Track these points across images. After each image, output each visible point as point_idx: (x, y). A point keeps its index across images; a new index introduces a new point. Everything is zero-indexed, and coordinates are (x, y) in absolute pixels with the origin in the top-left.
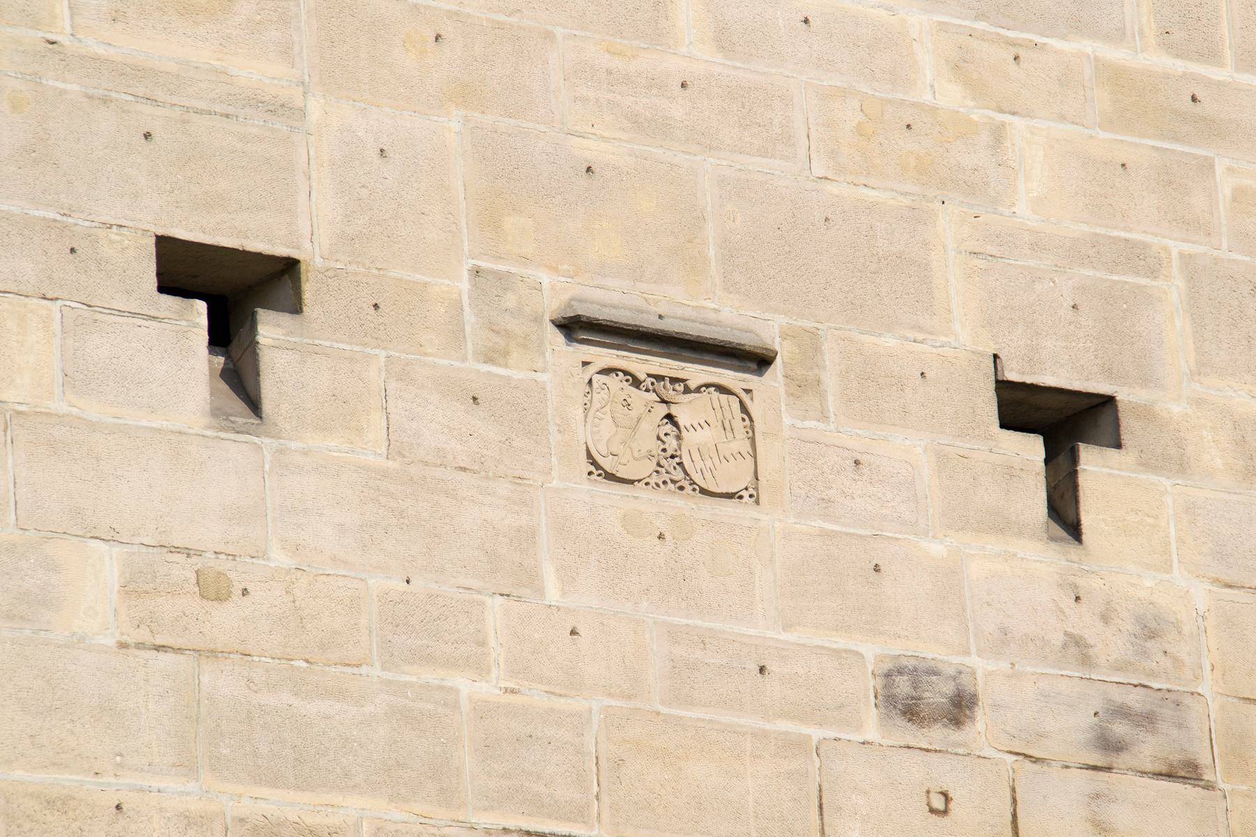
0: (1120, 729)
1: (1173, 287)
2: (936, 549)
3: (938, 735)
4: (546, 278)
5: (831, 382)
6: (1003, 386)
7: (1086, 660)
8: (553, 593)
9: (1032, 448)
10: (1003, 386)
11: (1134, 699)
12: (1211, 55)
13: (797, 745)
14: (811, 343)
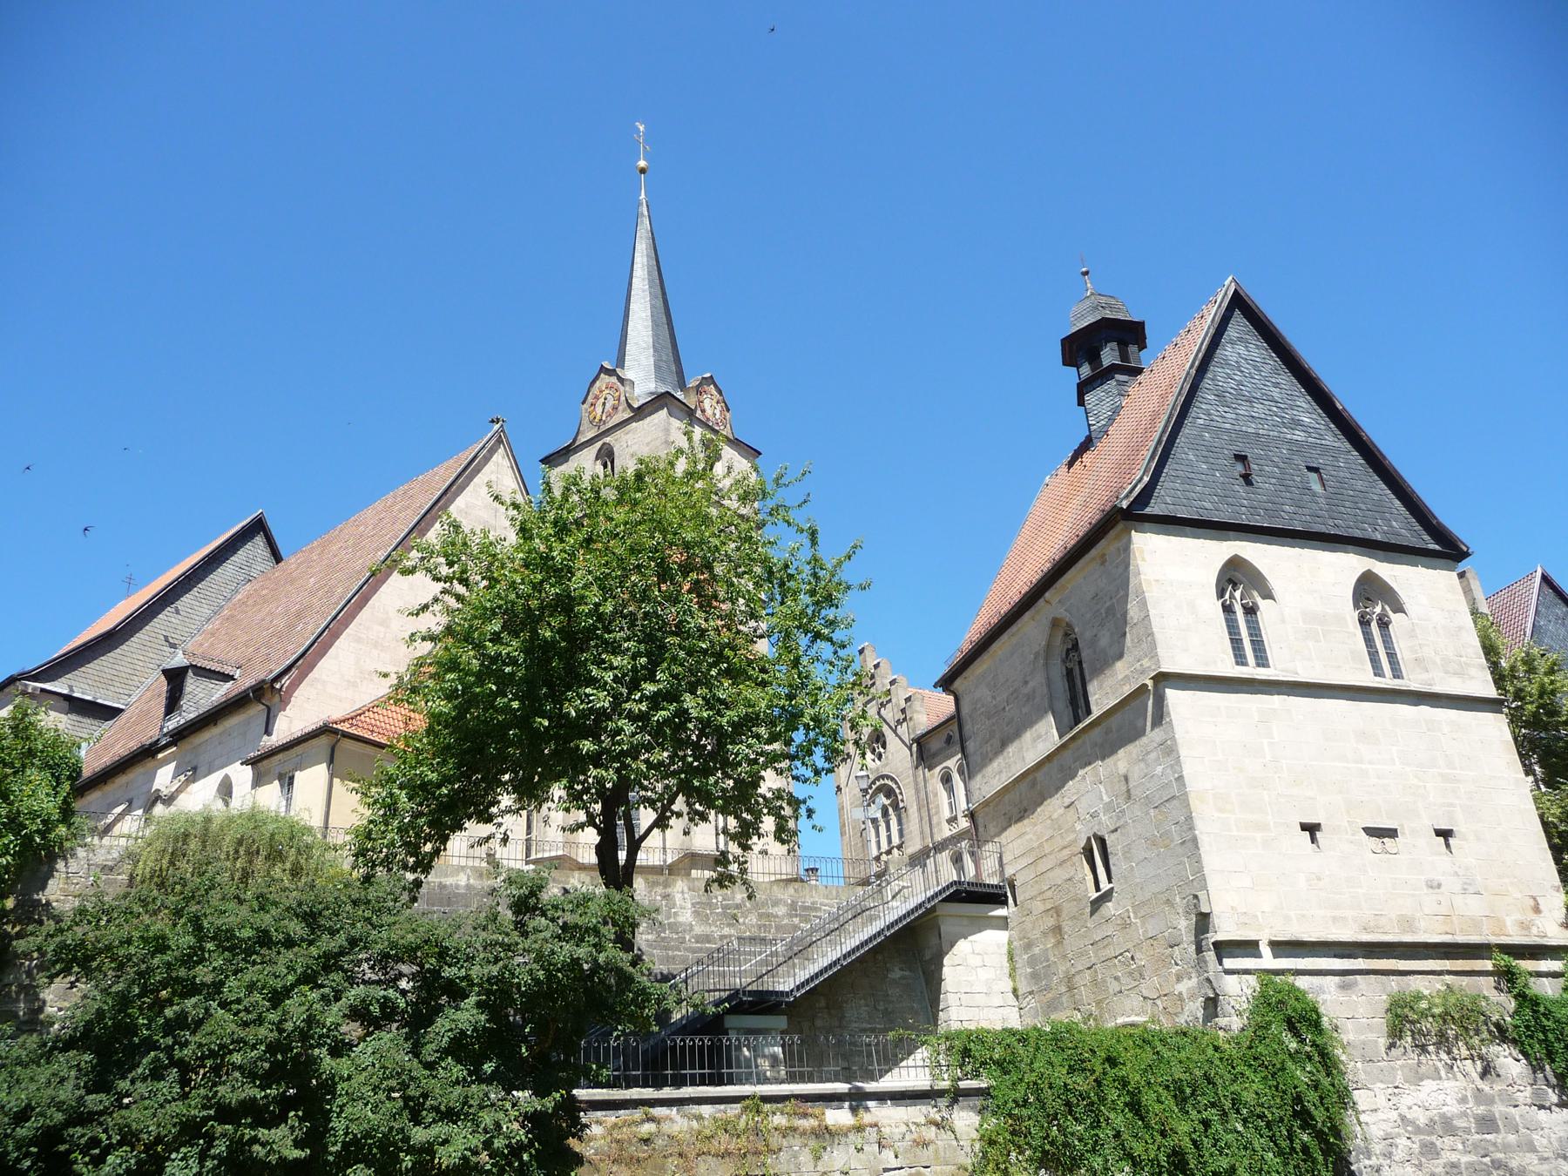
0: (1466, 886)
3: (1437, 890)
5: (1407, 832)
6: (1435, 830)
9: (1441, 839)
10: (1435, 830)
12: (1456, 769)
13: (1413, 895)
14: (1402, 826)
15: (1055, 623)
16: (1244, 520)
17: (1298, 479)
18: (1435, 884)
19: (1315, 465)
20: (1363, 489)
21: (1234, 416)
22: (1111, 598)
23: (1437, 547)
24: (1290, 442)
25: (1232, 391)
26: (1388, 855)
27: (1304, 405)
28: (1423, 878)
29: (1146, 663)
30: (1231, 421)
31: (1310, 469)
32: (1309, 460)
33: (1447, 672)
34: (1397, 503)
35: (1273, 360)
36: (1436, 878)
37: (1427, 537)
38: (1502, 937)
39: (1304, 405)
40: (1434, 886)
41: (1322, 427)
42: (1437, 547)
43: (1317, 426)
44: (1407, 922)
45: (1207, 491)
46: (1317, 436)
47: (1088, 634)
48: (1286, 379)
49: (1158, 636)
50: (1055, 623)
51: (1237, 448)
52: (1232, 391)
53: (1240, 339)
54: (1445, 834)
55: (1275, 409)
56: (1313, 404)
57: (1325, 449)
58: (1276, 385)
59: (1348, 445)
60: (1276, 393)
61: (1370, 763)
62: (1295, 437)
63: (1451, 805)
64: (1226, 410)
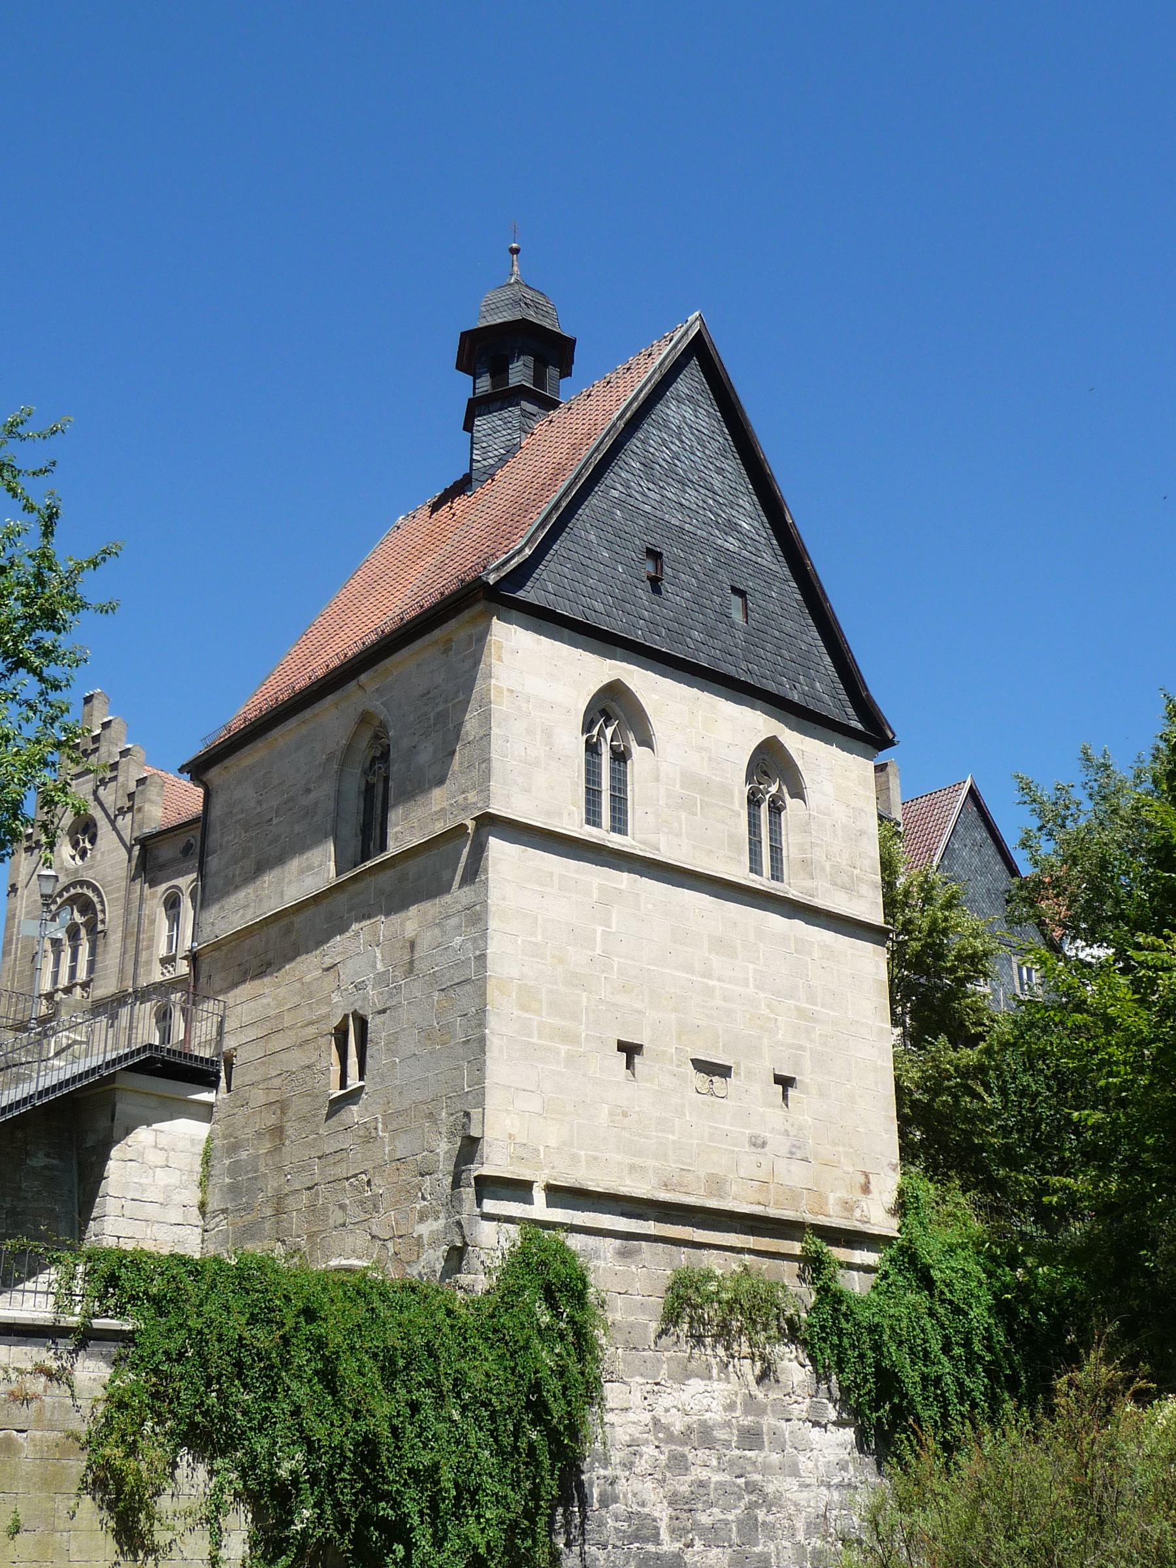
1: (807, 1054)
2: (761, 1110)
3: (759, 1150)
4: (689, 1049)
7: (788, 1135)
8: (688, 1118)
9: (780, 1088)
11: (796, 1143)
12: (816, 1005)
14: (738, 1064)
15: (365, 718)
16: (639, 636)
17: (718, 600)
18: (759, 1142)
19: (742, 587)
20: (792, 632)
21: (658, 497)
22: (446, 701)
23: (860, 726)
24: (720, 549)
25: (664, 464)
26: (713, 1099)
27: (747, 506)
28: (747, 1132)
29: (472, 797)
30: (653, 503)
31: (736, 591)
32: (737, 579)
33: (835, 884)
34: (827, 660)
35: (722, 438)
36: (763, 1134)
37: (851, 711)
38: (820, 1217)
39: (747, 506)
40: (758, 1143)
41: (763, 541)
42: (860, 726)
43: (757, 538)
44: (716, 1184)
45: (602, 587)
46: (754, 550)
47: (405, 743)
48: (733, 465)
49: (495, 765)
50: (365, 718)
51: (653, 541)
52: (664, 464)
53: (690, 398)
54: (785, 1082)
55: (711, 502)
56: (759, 507)
57: (759, 570)
58: (720, 471)
59: (788, 573)
60: (717, 482)
61: (719, 980)
62: (727, 545)
63: (801, 1048)
64: (651, 486)
